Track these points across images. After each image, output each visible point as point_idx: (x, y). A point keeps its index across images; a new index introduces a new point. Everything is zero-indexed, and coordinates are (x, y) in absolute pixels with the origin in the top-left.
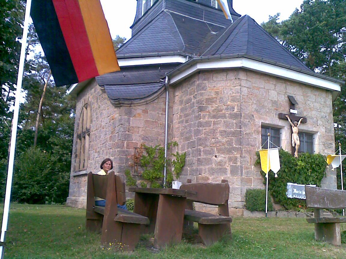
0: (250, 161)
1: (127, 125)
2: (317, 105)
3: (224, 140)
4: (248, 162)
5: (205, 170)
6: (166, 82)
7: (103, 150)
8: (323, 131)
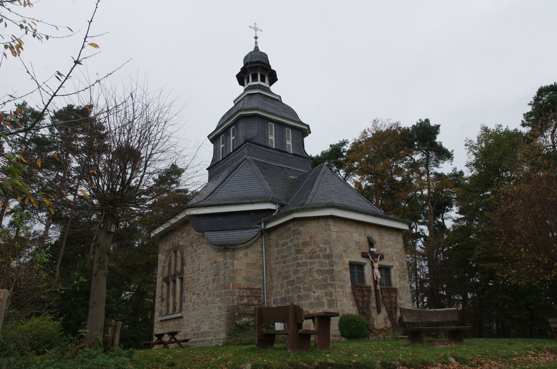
0: (343, 295)
1: (232, 267)
2: (390, 243)
3: (320, 278)
4: (341, 295)
5: (306, 304)
6: (263, 227)
7: (204, 292)
8: (397, 264)
